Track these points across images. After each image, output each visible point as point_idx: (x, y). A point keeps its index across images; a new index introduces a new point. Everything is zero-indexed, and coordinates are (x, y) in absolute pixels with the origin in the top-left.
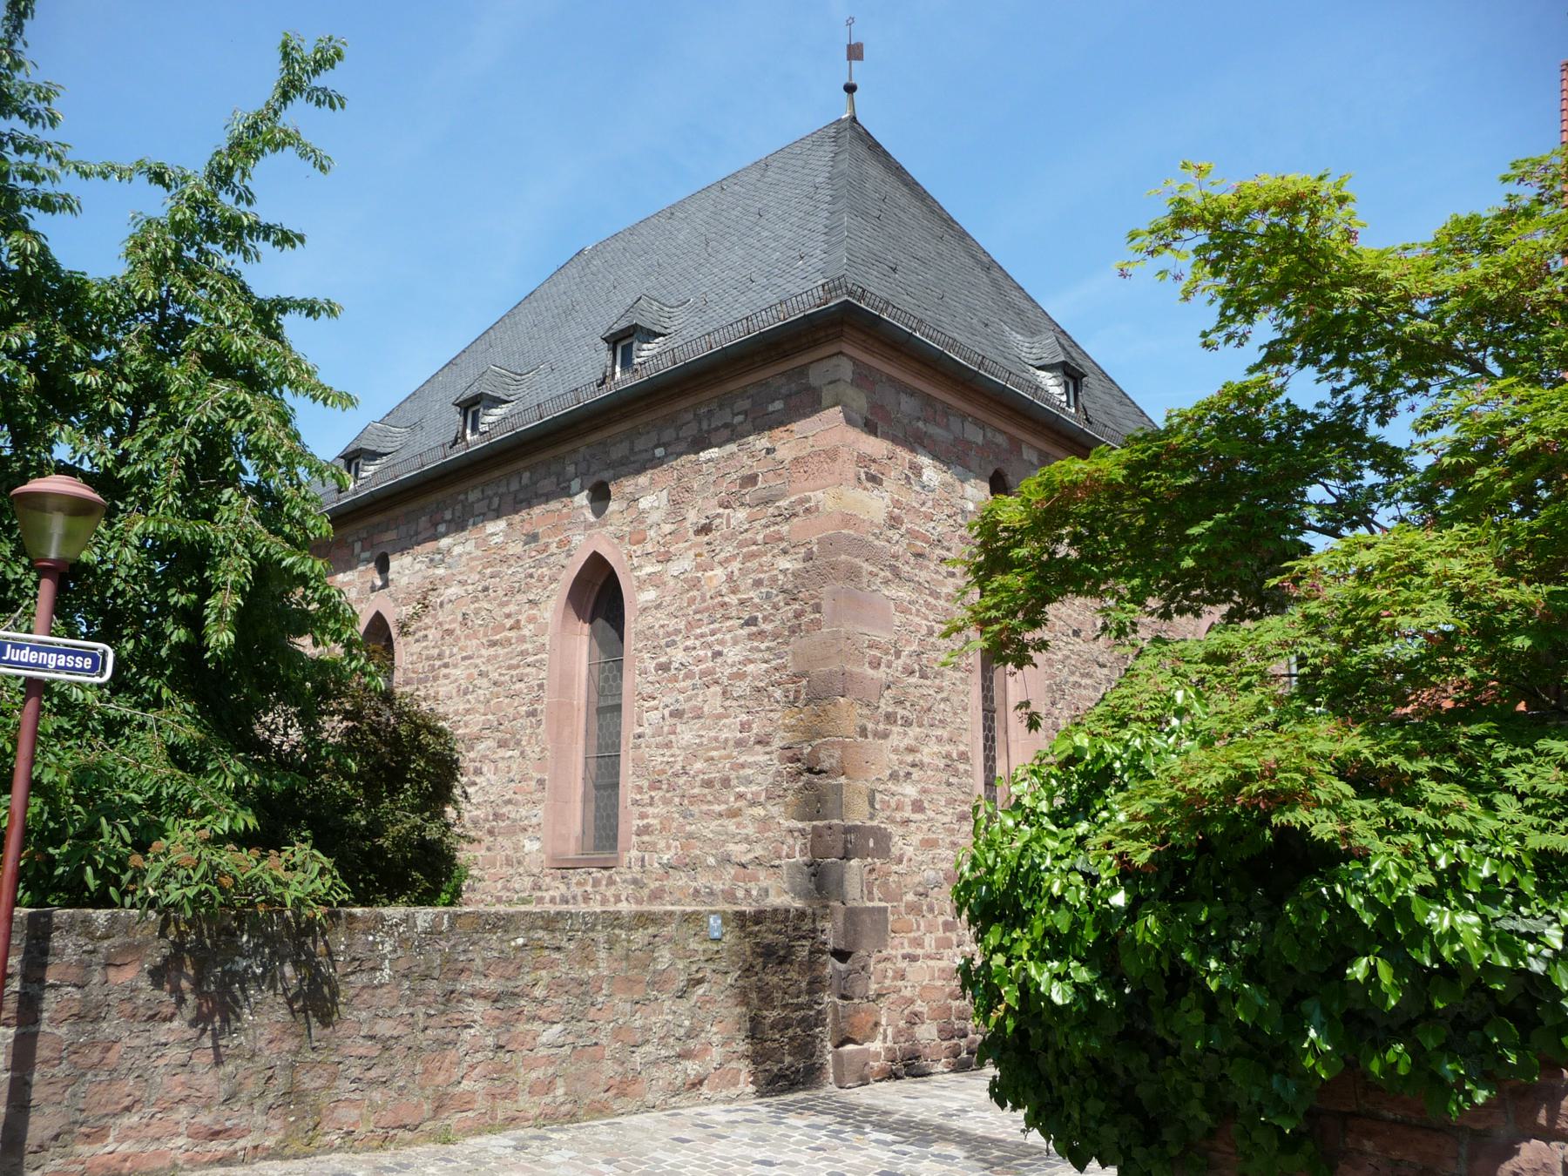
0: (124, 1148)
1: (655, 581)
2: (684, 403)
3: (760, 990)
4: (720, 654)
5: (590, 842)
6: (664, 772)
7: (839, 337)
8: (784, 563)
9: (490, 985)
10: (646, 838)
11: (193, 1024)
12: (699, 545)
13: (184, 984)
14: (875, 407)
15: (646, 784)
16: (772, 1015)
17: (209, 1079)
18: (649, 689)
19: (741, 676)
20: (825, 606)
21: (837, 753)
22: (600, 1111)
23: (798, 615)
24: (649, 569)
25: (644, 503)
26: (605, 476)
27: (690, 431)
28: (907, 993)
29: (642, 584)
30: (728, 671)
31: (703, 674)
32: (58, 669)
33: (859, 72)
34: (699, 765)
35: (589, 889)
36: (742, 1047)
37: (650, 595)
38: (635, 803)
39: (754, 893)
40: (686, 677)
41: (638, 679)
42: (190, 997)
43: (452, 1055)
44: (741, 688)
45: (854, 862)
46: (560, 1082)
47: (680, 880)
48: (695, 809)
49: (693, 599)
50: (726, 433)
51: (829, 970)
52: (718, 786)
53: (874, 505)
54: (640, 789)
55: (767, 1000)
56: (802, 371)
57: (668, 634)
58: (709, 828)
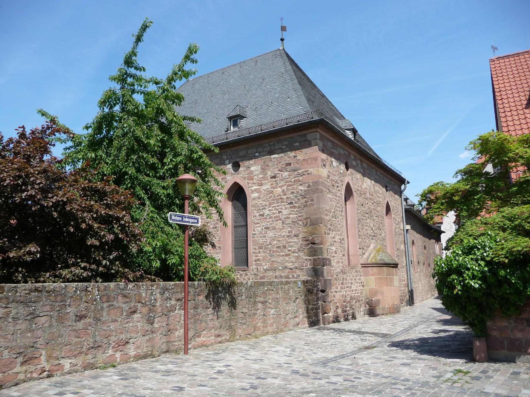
0: (204, 339)
1: (256, 191)
2: (265, 141)
3: (308, 300)
4: (281, 212)
5: (234, 264)
6: (263, 244)
7: (317, 127)
8: (301, 188)
9: (261, 299)
10: (258, 262)
11: (213, 309)
12: (271, 181)
13: (211, 300)
14: (324, 146)
15: (257, 247)
16: (310, 307)
17: (217, 323)
18: (257, 221)
19: (289, 218)
20: (315, 200)
21: (320, 239)
22: (282, 331)
23: (306, 202)
24: (255, 187)
25: (252, 169)
26: (238, 160)
27: (268, 149)
28: (336, 301)
29: (253, 192)
30: (284, 217)
31: (275, 217)
32: (192, 223)
33: (285, 35)
34: (275, 242)
35: (239, 277)
36: (306, 315)
37: (256, 195)
38: (254, 253)
39: (295, 276)
40: (270, 218)
41: (253, 218)
42: (212, 303)
43: (256, 317)
44: (289, 221)
45: (325, 267)
46: (275, 323)
47: (270, 273)
48: (274, 254)
49: (271, 197)
50: (280, 151)
51: (320, 295)
52: (282, 248)
53: (324, 172)
54: (255, 249)
55: (309, 303)
56: (305, 135)
57: (263, 206)
58: (280, 259)
